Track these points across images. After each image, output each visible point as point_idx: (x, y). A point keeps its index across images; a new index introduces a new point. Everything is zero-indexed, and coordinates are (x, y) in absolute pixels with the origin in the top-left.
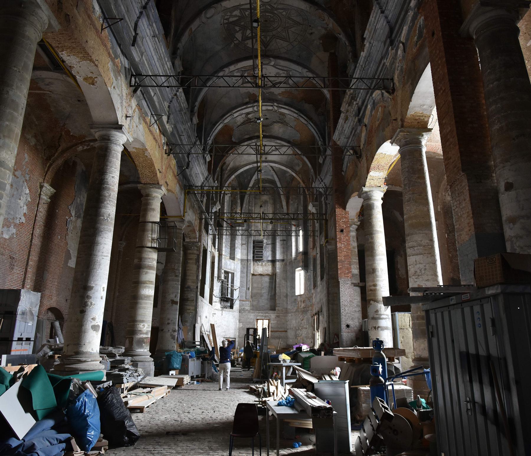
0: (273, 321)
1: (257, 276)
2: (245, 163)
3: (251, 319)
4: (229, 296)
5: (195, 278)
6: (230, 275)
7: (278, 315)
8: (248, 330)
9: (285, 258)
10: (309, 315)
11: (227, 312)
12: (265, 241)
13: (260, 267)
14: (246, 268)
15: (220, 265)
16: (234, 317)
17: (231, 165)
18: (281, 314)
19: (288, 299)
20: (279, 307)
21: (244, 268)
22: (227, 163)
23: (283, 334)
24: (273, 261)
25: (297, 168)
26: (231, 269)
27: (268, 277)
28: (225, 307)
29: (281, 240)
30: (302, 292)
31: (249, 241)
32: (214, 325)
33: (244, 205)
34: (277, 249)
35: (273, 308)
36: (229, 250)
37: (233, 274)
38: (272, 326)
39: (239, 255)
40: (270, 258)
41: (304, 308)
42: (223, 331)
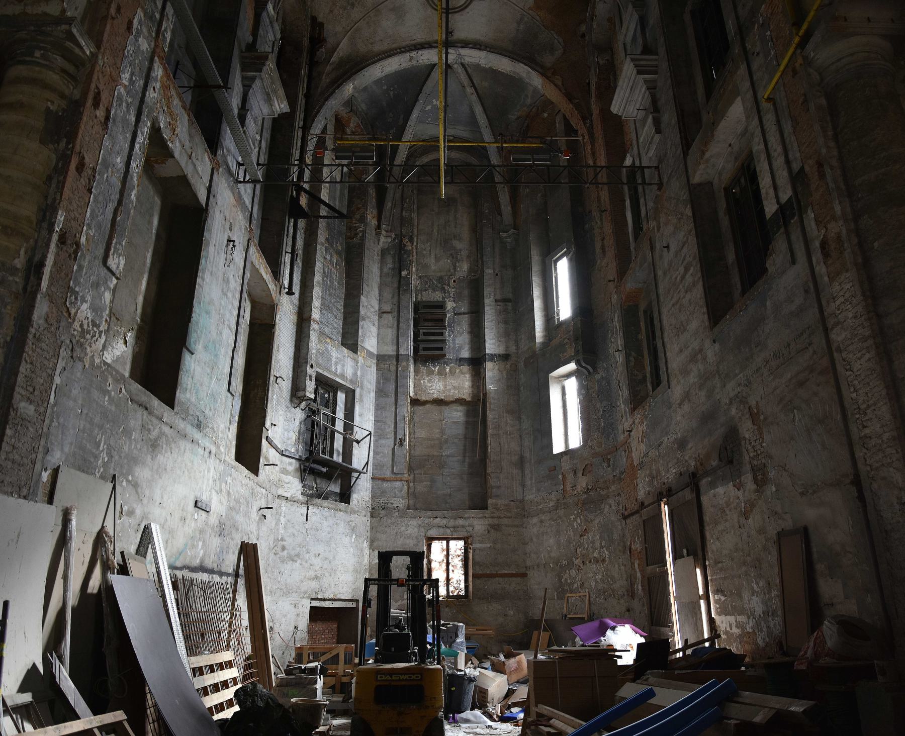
0: (481, 542)
1: (428, 406)
2: (385, 46)
3: (410, 537)
4: (338, 458)
5: (28, 210)
6: (341, 397)
7: (496, 521)
8: (385, 558)
9: (513, 349)
10: (610, 510)
11: (326, 512)
12: (450, 305)
13: (436, 378)
14: (393, 382)
15: (303, 351)
16: (353, 530)
17: (343, 49)
18: (506, 521)
19: (527, 472)
20: (497, 496)
21: (386, 380)
22: (331, 41)
23: (513, 585)
24: (477, 362)
25: (548, 60)
26: (342, 376)
27: (460, 408)
28: (321, 495)
29: (496, 301)
30: (576, 442)
31: (403, 303)
32: (255, 546)
33: (388, 205)
34: (487, 324)
35: (479, 502)
36: (341, 323)
37: (351, 395)
38: (477, 558)
39: (370, 339)
40: (466, 354)
41: (587, 491)
42: (312, 574)
